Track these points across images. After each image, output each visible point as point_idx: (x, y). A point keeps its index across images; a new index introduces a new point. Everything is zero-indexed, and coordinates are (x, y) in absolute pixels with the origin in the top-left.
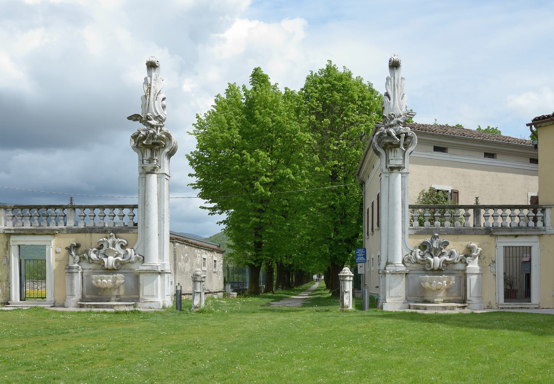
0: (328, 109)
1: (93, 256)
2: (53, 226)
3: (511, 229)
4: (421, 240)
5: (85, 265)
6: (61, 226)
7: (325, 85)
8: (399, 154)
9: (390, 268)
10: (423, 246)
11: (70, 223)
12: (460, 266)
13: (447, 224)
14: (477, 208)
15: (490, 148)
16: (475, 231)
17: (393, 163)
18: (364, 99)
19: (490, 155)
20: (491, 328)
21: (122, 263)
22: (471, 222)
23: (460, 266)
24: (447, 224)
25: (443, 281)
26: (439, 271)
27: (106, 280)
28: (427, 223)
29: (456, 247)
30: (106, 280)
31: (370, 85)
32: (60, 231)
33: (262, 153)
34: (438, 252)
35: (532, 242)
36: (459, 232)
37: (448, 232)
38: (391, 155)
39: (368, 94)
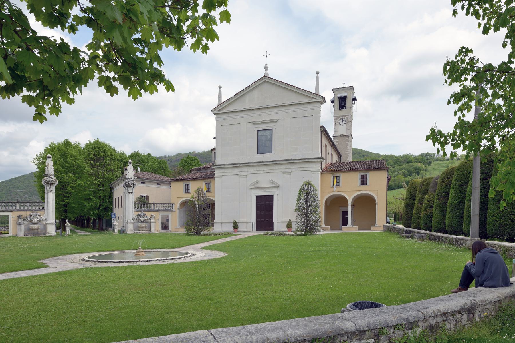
0: (98, 159)
1: (29, 219)
2: (11, 208)
3: (164, 210)
4: (138, 213)
5: (25, 222)
6: (14, 208)
7: (97, 149)
8: (131, 189)
9: (129, 222)
10: (139, 215)
11: (18, 208)
12: (149, 221)
13: (146, 208)
14: (154, 204)
15: (159, 182)
16: (154, 210)
17: (130, 191)
18: (113, 155)
19: (159, 184)
20: (24, 176)
21: (40, 221)
22: (152, 208)
23: (149, 221)
24: (146, 208)
25: (143, 225)
26: (143, 222)
27: (36, 227)
28: (140, 208)
29: (148, 214)
30: (36, 227)
31: (114, 148)
32: (14, 211)
33: (71, 175)
34: (143, 216)
35: (169, 214)
36: (149, 211)
37: (146, 211)
38: (129, 189)
39: (114, 153)
